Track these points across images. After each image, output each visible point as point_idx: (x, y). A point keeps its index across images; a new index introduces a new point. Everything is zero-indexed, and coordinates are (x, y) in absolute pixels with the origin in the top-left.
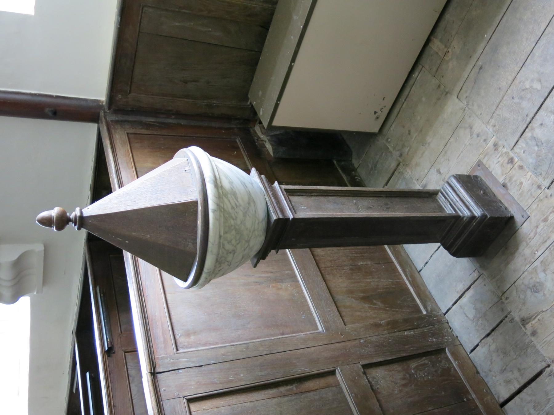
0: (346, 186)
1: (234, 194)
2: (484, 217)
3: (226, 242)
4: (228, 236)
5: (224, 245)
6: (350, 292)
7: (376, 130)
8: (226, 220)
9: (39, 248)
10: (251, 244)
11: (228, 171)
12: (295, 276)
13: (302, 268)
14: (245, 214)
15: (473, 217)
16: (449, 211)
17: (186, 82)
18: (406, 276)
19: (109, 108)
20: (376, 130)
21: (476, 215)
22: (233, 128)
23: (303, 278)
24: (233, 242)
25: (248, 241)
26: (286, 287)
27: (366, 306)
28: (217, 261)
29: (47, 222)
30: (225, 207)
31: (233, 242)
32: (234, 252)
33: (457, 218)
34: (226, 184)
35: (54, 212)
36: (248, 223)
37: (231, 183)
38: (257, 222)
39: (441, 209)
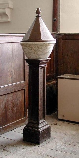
0: (46, 84)
1: (46, 49)
2: (39, 132)
3: (35, 47)
4: (37, 47)
5: (34, 46)
6: (8, 101)
7: (59, 117)
8: (41, 46)
9: (9, 20)
10: (34, 54)
11: (51, 49)
12: (13, 83)
13: (15, 86)
14: (42, 51)
15: (39, 128)
16: (40, 122)
17: (68, 55)
18: (11, 124)
19: (58, 34)
20: (59, 117)
21: (40, 129)
22: (54, 73)
23: (13, 85)
24: (35, 49)
25: (34, 53)
26: (9, 79)
27: (4, 106)
28: (30, 45)
29: (38, 9)
30: (44, 46)
31: (35, 49)
32: (32, 49)
33: (38, 124)
34: (49, 47)
35: (40, 11)
36: (39, 53)
37: (49, 48)
38: (39, 55)
39: (41, 120)
